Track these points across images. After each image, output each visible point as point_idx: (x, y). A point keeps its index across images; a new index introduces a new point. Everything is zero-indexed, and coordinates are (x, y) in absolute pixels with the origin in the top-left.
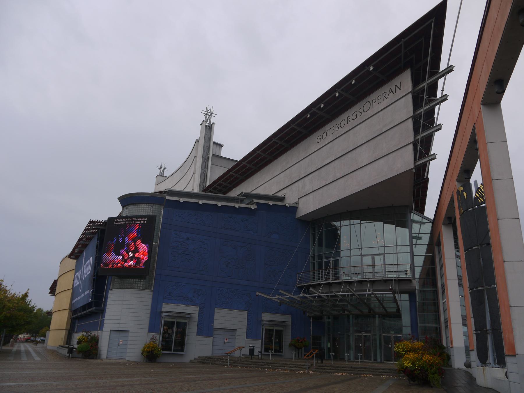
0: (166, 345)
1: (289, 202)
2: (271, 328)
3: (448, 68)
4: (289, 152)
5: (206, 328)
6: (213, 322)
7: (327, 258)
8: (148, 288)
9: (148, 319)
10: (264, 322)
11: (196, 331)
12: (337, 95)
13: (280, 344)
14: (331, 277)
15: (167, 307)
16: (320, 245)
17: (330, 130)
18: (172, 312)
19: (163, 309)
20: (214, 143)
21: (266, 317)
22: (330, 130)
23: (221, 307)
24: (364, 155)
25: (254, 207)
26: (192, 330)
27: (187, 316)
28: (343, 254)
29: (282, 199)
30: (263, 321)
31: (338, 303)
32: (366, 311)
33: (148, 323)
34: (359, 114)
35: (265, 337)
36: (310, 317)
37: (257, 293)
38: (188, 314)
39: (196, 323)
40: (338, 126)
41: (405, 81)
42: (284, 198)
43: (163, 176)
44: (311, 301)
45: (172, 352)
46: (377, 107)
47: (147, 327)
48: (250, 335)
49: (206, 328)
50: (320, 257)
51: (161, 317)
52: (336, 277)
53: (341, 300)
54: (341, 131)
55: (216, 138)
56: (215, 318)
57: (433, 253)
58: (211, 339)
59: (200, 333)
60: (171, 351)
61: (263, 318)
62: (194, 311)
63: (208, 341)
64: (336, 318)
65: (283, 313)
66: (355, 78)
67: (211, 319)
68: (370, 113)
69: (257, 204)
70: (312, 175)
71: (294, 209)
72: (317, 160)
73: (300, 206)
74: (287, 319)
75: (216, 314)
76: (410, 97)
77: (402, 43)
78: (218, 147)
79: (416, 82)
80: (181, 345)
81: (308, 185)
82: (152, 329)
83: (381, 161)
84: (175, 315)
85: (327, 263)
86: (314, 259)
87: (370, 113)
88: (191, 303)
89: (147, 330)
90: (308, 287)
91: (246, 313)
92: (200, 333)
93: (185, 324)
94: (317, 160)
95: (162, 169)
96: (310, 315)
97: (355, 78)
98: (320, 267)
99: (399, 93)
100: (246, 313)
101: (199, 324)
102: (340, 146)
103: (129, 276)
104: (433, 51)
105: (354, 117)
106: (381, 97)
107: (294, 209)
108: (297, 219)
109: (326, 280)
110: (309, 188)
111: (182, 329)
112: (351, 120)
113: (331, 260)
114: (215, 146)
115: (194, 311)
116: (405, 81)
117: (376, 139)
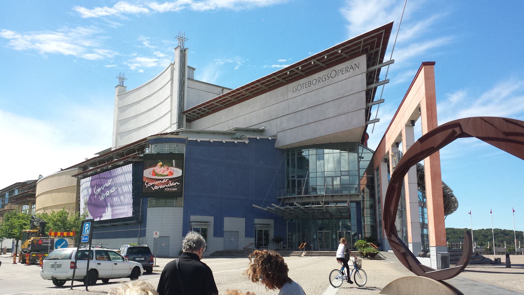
2: (262, 229)
3: (391, 60)
6: (222, 227)
7: (298, 178)
10: (193, 223)
12: (313, 63)
13: (267, 239)
15: (193, 218)
16: (294, 167)
17: (304, 85)
21: (257, 221)
22: (304, 85)
28: (311, 175)
29: (262, 131)
33: (182, 230)
34: (327, 78)
35: (479, 266)
37: (254, 205)
38: (207, 222)
39: (213, 229)
40: (310, 83)
41: (362, 60)
48: (247, 235)
49: (219, 232)
55: (189, 63)
57: (373, 174)
58: (222, 239)
59: (216, 235)
61: (255, 222)
62: (211, 219)
63: (220, 240)
69: (249, 139)
71: (274, 141)
73: (279, 137)
74: (271, 222)
76: (365, 76)
77: (362, 40)
88: (208, 214)
92: (216, 235)
95: (122, 79)
98: (294, 186)
100: (244, 219)
103: (163, 196)
104: (397, 195)
105: (324, 80)
106: (344, 70)
108: (277, 148)
115: (211, 219)
116: (362, 60)
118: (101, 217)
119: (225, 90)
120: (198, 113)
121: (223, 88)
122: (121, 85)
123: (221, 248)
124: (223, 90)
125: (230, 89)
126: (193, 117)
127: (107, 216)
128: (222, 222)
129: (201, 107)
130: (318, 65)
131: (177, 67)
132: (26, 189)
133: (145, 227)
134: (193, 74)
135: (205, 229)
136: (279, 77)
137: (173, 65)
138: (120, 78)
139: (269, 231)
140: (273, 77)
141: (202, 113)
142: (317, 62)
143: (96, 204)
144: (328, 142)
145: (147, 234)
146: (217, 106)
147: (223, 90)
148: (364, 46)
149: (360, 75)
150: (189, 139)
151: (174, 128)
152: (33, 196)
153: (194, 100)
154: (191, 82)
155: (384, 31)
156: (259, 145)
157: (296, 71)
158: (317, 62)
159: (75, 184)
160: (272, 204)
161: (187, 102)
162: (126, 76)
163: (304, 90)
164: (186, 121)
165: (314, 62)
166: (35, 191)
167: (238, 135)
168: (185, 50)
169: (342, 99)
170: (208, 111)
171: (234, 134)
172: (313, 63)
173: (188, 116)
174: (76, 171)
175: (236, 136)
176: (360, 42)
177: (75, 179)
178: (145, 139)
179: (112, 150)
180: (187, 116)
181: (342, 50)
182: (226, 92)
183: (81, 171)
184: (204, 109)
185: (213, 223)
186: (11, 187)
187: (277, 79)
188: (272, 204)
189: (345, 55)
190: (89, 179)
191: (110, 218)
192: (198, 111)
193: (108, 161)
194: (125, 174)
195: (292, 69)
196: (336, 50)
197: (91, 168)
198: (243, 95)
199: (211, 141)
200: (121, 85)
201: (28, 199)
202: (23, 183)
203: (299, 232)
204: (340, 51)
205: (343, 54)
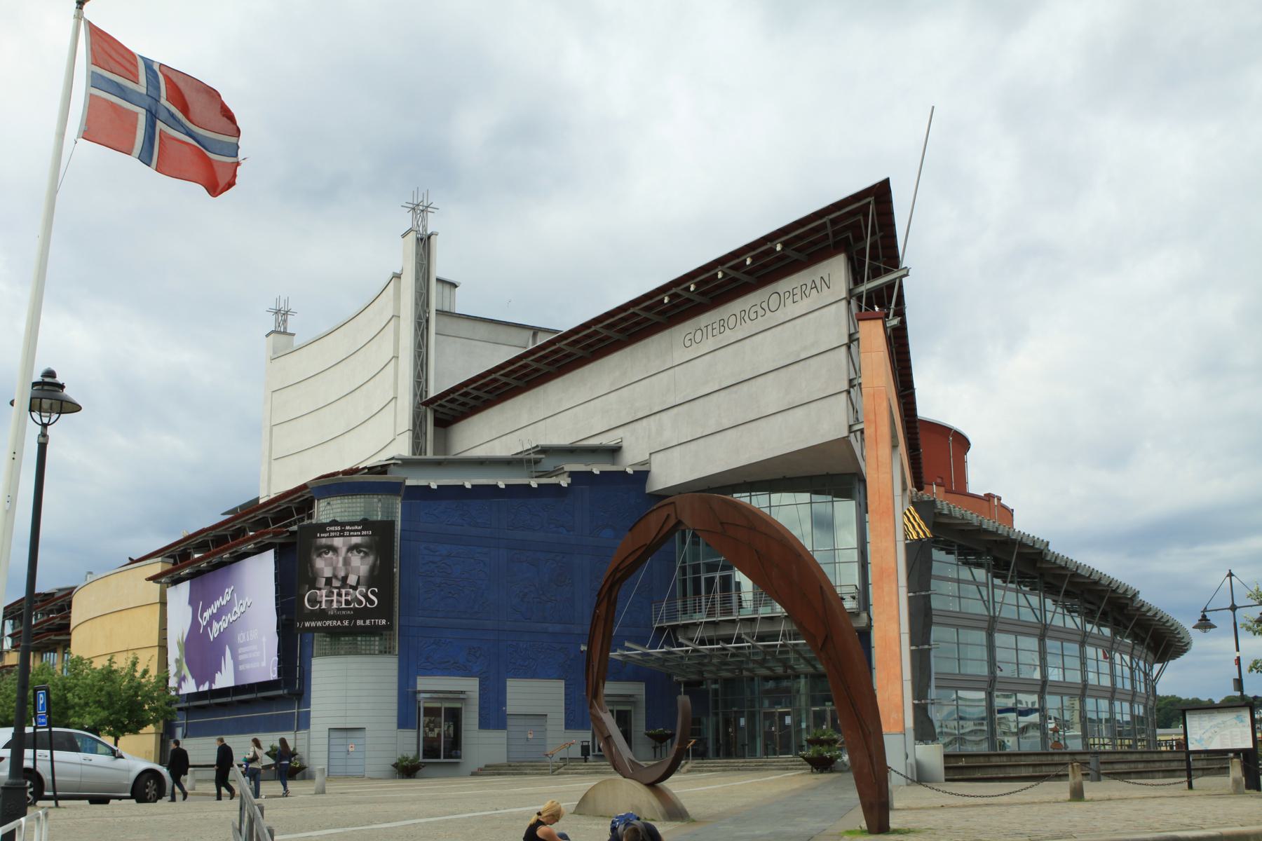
0: (431, 750)
1: (629, 461)
4: (628, 350)
5: (493, 716)
6: (504, 704)
7: (708, 571)
8: (384, 652)
9: (395, 706)
10: (423, 695)
11: (476, 721)
12: (720, 275)
14: (718, 607)
15: (426, 684)
18: (450, 692)
19: (419, 688)
20: (438, 280)
23: (515, 676)
24: (771, 394)
25: (564, 482)
26: (471, 719)
27: (459, 696)
29: (614, 452)
30: (420, 692)
31: (729, 659)
32: (780, 670)
34: (761, 312)
36: (679, 683)
38: (462, 692)
39: (476, 708)
40: (723, 323)
42: (620, 448)
43: (285, 333)
44: (682, 657)
45: (442, 760)
46: (792, 310)
47: (395, 720)
49: (493, 716)
50: (696, 569)
51: (416, 701)
52: (728, 611)
53: (733, 655)
54: (730, 336)
55: (441, 267)
56: (509, 696)
59: (484, 724)
60: (439, 757)
62: (470, 686)
64: (727, 682)
65: (629, 679)
66: (753, 253)
67: (502, 701)
68: (781, 316)
69: (572, 474)
70: (676, 410)
71: (642, 476)
72: (688, 381)
73: (655, 469)
74: (637, 690)
75: (509, 690)
78: (447, 289)
79: (857, 276)
80: (454, 745)
81: (670, 428)
82: (405, 721)
83: (799, 411)
84: (441, 695)
85: (710, 581)
86: (684, 574)
87: (781, 316)
88: (465, 672)
89: (395, 726)
90: (674, 629)
91: (561, 685)
92: (484, 724)
93: (460, 709)
94: (688, 381)
95: (282, 314)
96: (680, 679)
97: (753, 253)
98: (697, 592)
99: (827, 295)
100: (562, 684)
101: (481, 708)
102: (728, 366)
105: (753, 316)
106: (797, 291)
107: (642, 476)
109: (709, 615)
110: (670, 437)
111: (454, 716)
112: (746, 318)
113: (718, 575)
114: (440, 286)
115: (470, 686)
116: (836, 271)
117: (791, 368)
118: (212, 681)
119: (540, 335)
120: (463, 404)
121: (536, 331)
122: (281, 331)
123: (500, 757)
124: (535, 335)
125: (556, 332)
126: (451, 412)
127: (224, 679)
128: (502, 692)
129: (455, 395)
130: (734, 280)
131: (409, 282)
132: (51, 612)
133: (309, 705)
134: (452, 300)
135: (626, 712)
136: (647, 309)
137: (397, 276)
138: (277, 312)
139: (460, 709)
140: (493, 376)
141: (472, 403)
142: (733, 274)
143: (203, 652)
144: (781, 476)
145: (312, 721)
146: (536, 370)
147: (535, 335)
148: (835, 234)
149: (834, 306)
150: (409, 482)
151: (403, 448)
152: (65, 628)
153: (457, 365)
154: (446, 319)
155: (871, 199)
156: (606, 487)
157: (686, 295)
158: (733, 274)
159: (156, 597)
160: (627, 644)
161: (436, 374)
162: (292, 307)
163: (710, 344)
164: (435, 425)
165: (725, 275)
166: (68, 617)
167: (548, 463)
168: (429, 237)
169: (795, 366)
170: (486, 396)
171: (537, 462)
172: (720, 275)
173: (445, 410)
174: (156, 567)
175: (541, 467)
176: (823, 226)
177: (155, 588)
178: (304, 487)
179: (261, 501)
180: (435, 411)
181: (785, 245)
182: (542, 339)
183: (169, 566)
184: (475, 393)
185: (477, 695)
186: (16, 607)
187: (644, 315)
188: (627, 644)
189: (795, 256)
190: (185, 587)
191: (232, 684)
192: (462, 399)
193: (234, 537)
194: (258, 576)
195: (674, 290)
196: (769, 245)
197: (196, 556)
198: (601, 340)
199: (468, 485)
200: (281, 331)
201: (53, 637)
202: (46, 595)
203: (716, 714)
204: (779, 248)
205: (789, 252)
